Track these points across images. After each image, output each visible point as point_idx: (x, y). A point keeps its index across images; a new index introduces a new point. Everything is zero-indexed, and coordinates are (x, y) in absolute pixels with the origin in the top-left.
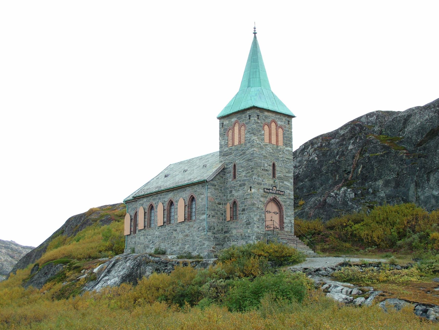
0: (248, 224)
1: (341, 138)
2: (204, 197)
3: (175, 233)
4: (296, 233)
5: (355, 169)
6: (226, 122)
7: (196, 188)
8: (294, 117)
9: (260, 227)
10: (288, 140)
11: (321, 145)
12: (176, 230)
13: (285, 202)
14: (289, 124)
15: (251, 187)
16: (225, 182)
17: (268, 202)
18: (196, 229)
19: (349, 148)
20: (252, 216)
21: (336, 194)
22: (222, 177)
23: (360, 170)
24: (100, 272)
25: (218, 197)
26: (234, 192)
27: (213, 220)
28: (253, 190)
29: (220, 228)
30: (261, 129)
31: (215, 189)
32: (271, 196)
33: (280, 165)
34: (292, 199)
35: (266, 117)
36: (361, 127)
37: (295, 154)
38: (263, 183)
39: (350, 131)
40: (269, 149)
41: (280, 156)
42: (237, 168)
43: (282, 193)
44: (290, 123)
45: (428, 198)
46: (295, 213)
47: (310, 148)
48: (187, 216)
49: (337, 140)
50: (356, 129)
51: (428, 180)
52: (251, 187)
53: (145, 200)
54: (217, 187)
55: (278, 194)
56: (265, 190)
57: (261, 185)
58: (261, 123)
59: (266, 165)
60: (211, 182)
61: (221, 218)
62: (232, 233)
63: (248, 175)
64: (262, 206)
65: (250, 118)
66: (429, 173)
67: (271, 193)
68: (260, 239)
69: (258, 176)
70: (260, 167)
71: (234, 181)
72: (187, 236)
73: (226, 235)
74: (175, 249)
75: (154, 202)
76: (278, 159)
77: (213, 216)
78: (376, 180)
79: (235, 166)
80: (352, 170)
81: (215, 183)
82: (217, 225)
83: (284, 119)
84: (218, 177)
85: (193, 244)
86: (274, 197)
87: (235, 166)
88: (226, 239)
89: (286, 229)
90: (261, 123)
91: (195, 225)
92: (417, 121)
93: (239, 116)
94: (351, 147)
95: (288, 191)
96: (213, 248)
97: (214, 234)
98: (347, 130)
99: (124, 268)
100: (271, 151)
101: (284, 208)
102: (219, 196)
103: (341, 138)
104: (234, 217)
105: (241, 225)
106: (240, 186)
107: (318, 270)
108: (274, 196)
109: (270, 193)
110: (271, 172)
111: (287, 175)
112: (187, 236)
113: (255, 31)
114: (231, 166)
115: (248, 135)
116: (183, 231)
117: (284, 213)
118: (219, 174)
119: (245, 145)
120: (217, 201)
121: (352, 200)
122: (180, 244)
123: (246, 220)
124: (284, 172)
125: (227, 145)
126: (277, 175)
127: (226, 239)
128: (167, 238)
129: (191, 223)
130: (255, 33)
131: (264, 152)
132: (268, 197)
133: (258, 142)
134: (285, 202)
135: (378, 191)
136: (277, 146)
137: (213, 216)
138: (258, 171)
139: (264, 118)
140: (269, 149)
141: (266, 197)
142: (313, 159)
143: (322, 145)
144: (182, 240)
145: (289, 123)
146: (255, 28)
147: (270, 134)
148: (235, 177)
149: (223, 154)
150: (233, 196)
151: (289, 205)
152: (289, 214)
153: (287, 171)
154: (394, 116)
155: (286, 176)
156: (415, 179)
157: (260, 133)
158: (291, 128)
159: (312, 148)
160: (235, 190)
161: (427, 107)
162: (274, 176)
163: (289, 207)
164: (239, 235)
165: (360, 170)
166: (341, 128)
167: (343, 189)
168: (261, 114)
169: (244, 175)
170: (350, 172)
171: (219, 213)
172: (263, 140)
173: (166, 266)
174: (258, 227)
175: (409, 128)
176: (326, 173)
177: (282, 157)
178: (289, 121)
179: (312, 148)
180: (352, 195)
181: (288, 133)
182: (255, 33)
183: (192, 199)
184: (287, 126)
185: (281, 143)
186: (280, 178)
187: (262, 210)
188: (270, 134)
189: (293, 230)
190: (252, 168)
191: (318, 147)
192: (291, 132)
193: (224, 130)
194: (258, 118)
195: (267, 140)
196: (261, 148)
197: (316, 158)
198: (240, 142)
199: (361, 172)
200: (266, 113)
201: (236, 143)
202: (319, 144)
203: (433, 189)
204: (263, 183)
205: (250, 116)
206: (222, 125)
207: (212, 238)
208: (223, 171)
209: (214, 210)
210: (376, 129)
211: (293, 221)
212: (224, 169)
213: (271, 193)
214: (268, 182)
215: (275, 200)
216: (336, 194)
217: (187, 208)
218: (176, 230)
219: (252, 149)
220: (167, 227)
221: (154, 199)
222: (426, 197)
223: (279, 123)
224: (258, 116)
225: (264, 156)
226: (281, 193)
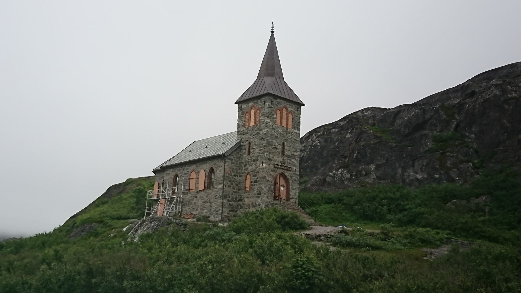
0: (259, 194)
3: (195, 200)
4: (300, 204)
5: (351, 154)
6: (244, 106)
7: (215, 161)
10: (297, 125)
11: (323, 133)
12: (196, 197)
15: (263, 163)
16: (241, 157)
18: (213, 197)
19: (347, 136)
20: (263, 187)
21: (334, 174)
22: (239, 153)
24: (128, 230)
26: (248, 166)
27: (229, 189)
28: (264, 165)
29: (234, 197)
30: (274, 113)
31: (232, 163)
32: (280, 171)
35: (279, 103)
36: (357, 119)
37: (302, 140)
39: (348, 122)
40: (280, 130)
42: (251, 145)
43: (289, 169)
45: (412, 181)
46: (299, 188)
47: (314, 135)
48: (206, 185)
49: (337, 130)
50: (352, 121)
51: (413, 166)
52: (263, 163)
53: (171, 170)
55: (286, 170)
59: (277, 144)
62: (245, 201)
63: (261, 152)
65: (264, 104)
66: (414, 160)
69: (270, 153)
71: (249, 157)
72: (205, 202)
73: (240, 203)
74: (194, 213)
75: (179, 173)
76: (287, 140)
78: (369, 164)
79: (250, 143)
81: (232, 157)
84: (235, 152)
85: (211, 210)
87: (250, 143)
88: (239, 207)
89: (291, 200)
91: (213, 193)
92: (405, 116)
93: (255, 101)
94: (348, 136)
95: (295, 168)
96: (228, 214)
98: (345, 122)
99: (148, 228)
100: (282, 132)
101: (290, 182)
106: (254, 161)
107: (319, 236)
108: (282, 171)
111: (295, 154)
112: (205, 202)
114: (247, 143)
115: (262, 118)
116: (202, 199)
118: (236, 150)
119: (260, 126)
121: (347, 179)
122: (199, 209)
125: (244, 125)
126: (286, 153)
127: (239, 207)
128: (189, 203)
129: (210, 192)
131: (275, 133)
134: (291, 177)
135: (370, 174)
136: (287, 129)
138: (270, 149)
140: (280, 130)
141: (275, 172)
142: (316, 145)
143: (323, 132)
144: (201, 205)
145: (299, 110)
147: (281, 118)
148: (249, 153)
149: (239, 133)
150: (247, 169)
151: (295, 180)
152: (294, 187)
153: (294, 150)
154: (386, 112)
156: (402, 164)
159: (315, 135)
160: (249, 165)
161: (414, 105)
163: (295, 181)
164: (250, 203)
166: (340, 120)
167: (340, 170)
168: (274, 101)
170: (346, 157)
172: (275, 122)
174: (267, 197)
175: (398, 122)
176: (327, 156)
177: (291, 139)
179: (315, 135)
180: (348, 176)
184: (296, 112)
185: (290, 127)
186: (288, 156)
188: (281, 118)
189: (297, 202)
190: (264, 146)
191: (321, 135)
193: (242, 112)
194: (272, 104)
195: (278, 123)
196: (273, 129)
197: (319, 144)
198: (255, 123)
200: (279, 100)
201: (252, 124)
202: (321, 133)
203: (417, 173)
205: (265, 101)
206: (240, 109)
208: (238, 147)
210: (370, 121)
211: (297, 194)
212: (240, 146)
214: (278, 159)
215: (282, 175)
216: (334, 174)
217: (207, 178)
218: (196, 197)
219: (266, 130)
221: (179, 170)
222: (411, 180)
223: (289, 109)
224: (272, 101)
226: (289, 169)
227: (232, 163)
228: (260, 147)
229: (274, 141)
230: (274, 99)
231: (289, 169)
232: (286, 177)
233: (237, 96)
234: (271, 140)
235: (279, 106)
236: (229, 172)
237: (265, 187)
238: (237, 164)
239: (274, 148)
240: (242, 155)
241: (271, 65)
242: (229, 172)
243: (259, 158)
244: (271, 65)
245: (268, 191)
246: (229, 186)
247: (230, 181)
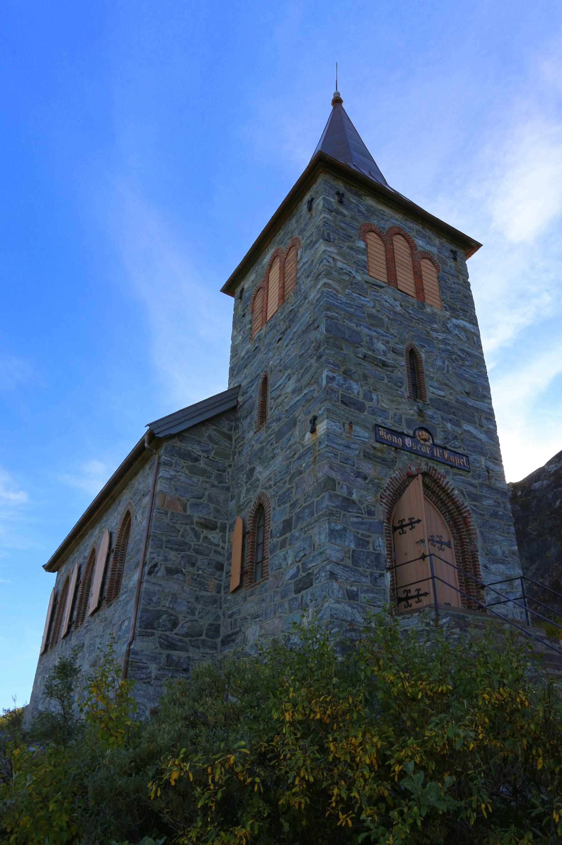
0: (304, 583)
1: (552, 478)
22: (230, 438)
25: (204, 500)
27: (173, 586)
28: (322, 427)
29: (205, 623)
38: (368, 404)
41: (435, 335)
43: (457, 461)
49: (545, 482)
54: (202, 464)
56: (382, 432)
64: (370, 498)
67: (410, 451)
77: (171, 572)
81: (196, 449)
82: (192, 612)
84: (210, 431)
97: (171, 646)
101: (474, 521)
102: (210, 499)
103: (552, 478)
104: (252, 572)
105: (278, 598)
109: (404, 448)
110: (402, 372)
117: (479, 544)
120: (197, 516)
123: (293, 571)
124: (458, 388)
126: (432, 390)
132: (399, 465)
133: (340, 265)
134: (475, 498)
137: (171, 572)
141: (389, 464)
151: (495, 515)
155: (465, 404)
162: (417, 391)
169: (289, 389)
171: (201, 561)
172: (364, 267)
184: (451, 263)
186: (441, 405)
194: (341, 202)
195: (379, 272)
207: (153, 668)
209: (181, 546)
213: (410, 451)
225: (370, 316)
227: (193, 471)
231: (457, 461)
232: (450, 497)
237: (333, 534)
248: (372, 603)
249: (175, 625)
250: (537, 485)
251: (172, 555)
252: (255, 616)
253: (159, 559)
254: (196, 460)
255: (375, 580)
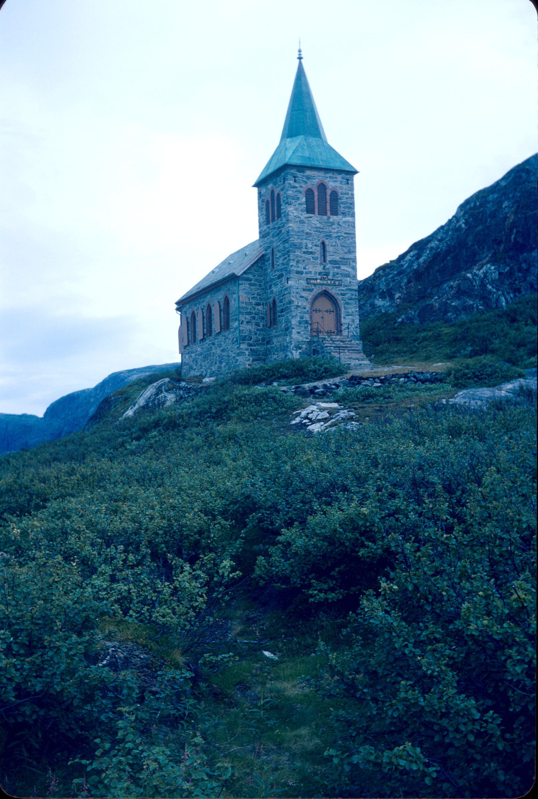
2: (242, 295)
8: (356, 172)
9: (302, 333)
13: (343, 295)
14: (348, 184)
17: (316, 298)
18: (230, 342)
22: (262, 268)
23: (513, 237)
27: (249, 327)
29: (260, 338)
31: (250, 285)
33: (334, 244)
34: (355, 290)
35: (308, 178)
41: (333, 231)
44: (350, 182)
48: (222, 324)
54: (253, 282)
57: (302, 274)
58: (301, 187)
59: (310, 246)
60: (245, 275)
61: (261, 324)
64: (305, 304)
68: (300, 348)
70: (300, 248)
77: (248, 322)
80: (504, 237)
81: (250, 276)
82: (256, 334)
83: (339, 177)
86: (324, 289)
90: (301, 187)
91: (230, 336)
95: (348, 279)
101: (341, 303)
110: (318, 254)
113: (300, 55)
126: (329, 258)
129: (226, 333)
130: (300, 58)
133: (295, 214)
134: (343, 295)
139: (305, 180)
141: (311, 290)
145: (349, 182)
146: (300, 51)
148: (273, 267)
151: (351, 299)
152: (350, 311)
155: (344, 258)
157: (299, 202)
158: (352, 189)
165: (513, 237)
168: (299, 175)
173: (189, 393)
174: (298, 333)
177: (337, 232)
178: (348, 180)
181: (347, 196)
182: (300, 58)
183: (227, 301)
184: (345, 187)
186: (333, 262)
187: (305, 308)
192: (353, 195)
194: (295, 181)
197: (463, 226)
199: (515, 239)
200: (308, 173)
204: (304, 271)
218: (214, 344)
220: (207, 341)
221: (195, 305)
224: (295, 177)
225: (307, 233)
228: (284, 255)
229: (305, 241)
230: (299, 171)
233: (255, 179)
234: (299, 241)
235: (309, 183)
236: (247, 300)
238: (260, 286)
239: (304, 252)
240: (266, 270)
241: (302, 117)
242: (247, 300)
243: (284, 273)
244: (302, 117)
245: (300, 323)
246: (248, 322)
247: (250, 313)
248: (305, 334)
249: (251, 339)
250: (491, 197)
251: (247, 316)
252: (275, 336)
253: (243, 319)
254: (251, 280)
255: (305, 328)
